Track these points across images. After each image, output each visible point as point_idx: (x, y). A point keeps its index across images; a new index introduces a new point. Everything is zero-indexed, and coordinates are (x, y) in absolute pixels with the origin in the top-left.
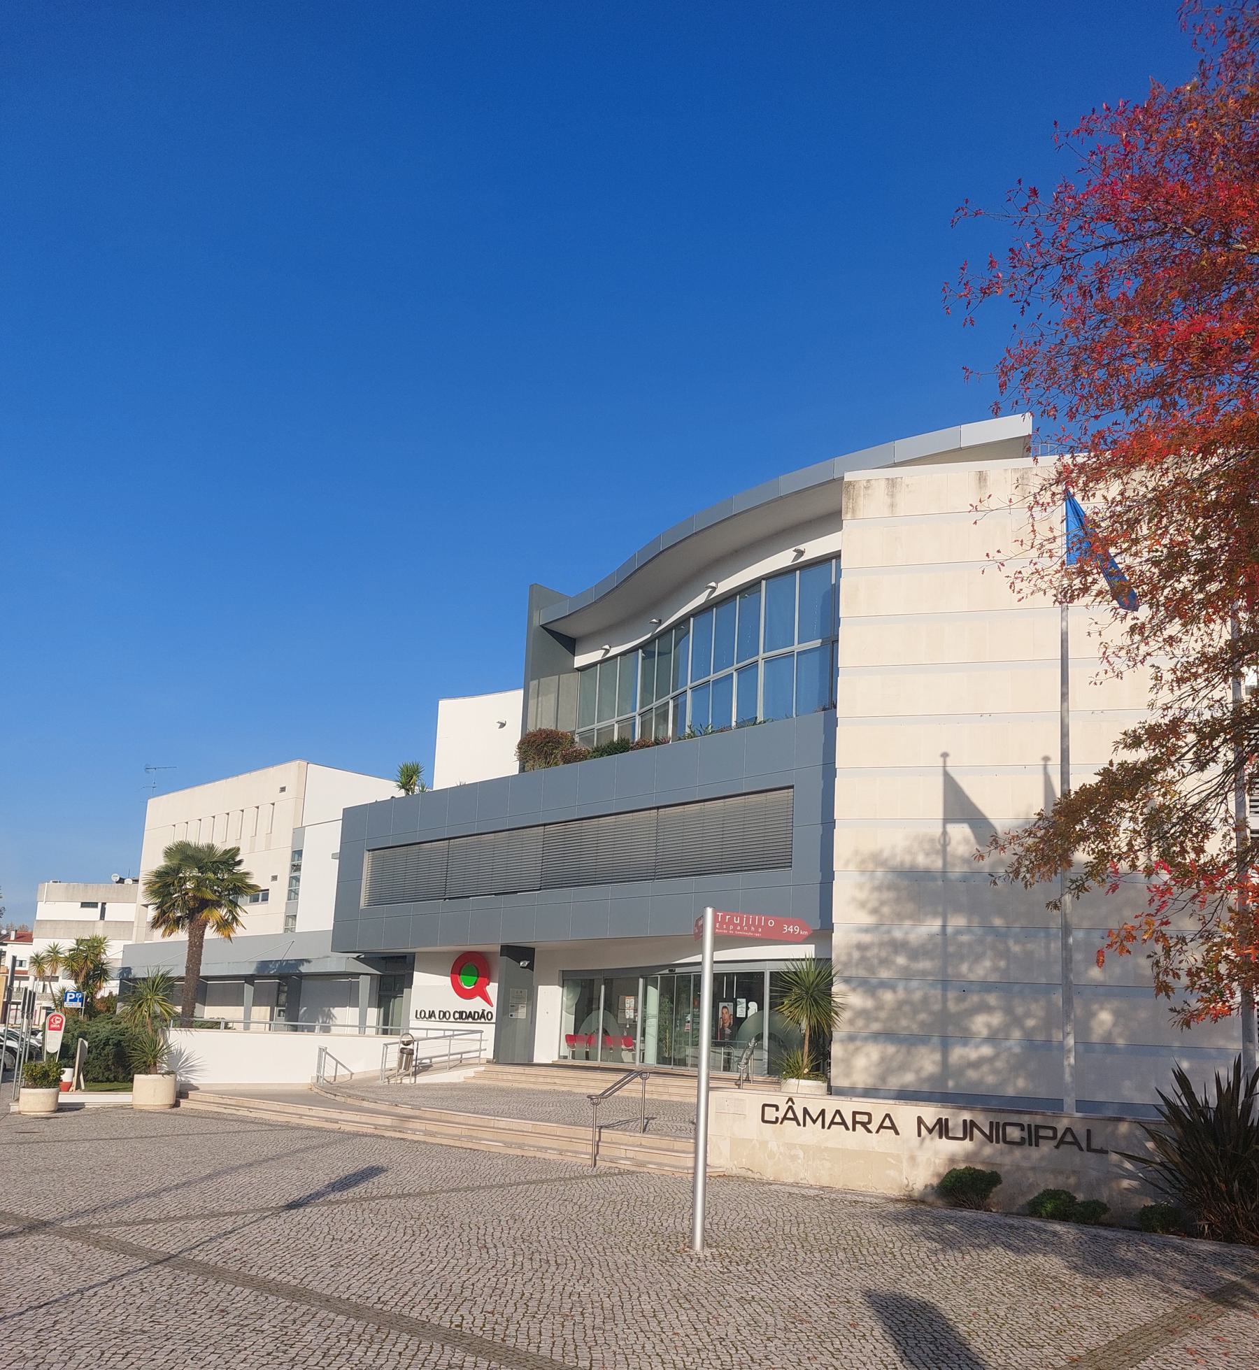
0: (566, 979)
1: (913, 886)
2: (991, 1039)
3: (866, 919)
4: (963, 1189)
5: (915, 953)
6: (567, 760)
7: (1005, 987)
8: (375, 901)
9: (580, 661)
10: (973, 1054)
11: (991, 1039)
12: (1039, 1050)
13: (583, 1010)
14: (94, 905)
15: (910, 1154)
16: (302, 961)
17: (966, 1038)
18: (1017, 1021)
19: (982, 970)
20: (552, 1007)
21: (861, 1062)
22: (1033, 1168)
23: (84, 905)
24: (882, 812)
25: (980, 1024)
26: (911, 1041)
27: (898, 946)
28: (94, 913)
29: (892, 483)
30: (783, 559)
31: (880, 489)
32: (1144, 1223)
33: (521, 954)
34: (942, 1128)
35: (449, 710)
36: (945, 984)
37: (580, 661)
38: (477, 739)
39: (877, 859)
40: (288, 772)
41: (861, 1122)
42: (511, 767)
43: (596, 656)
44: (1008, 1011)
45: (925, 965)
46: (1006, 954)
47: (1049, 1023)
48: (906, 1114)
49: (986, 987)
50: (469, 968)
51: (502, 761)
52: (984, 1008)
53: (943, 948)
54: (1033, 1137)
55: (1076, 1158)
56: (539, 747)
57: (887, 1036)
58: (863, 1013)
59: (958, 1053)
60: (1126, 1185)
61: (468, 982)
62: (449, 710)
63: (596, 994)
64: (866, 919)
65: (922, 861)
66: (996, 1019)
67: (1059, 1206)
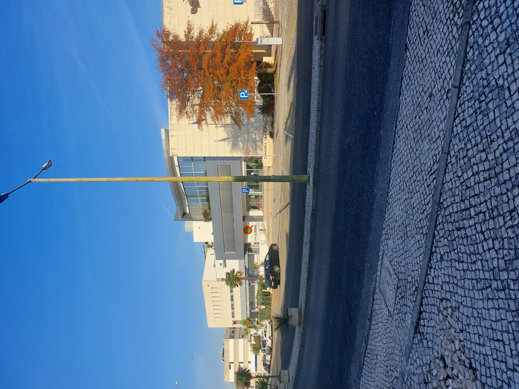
0: (248, 210)
1: (235, 146)
2: (255, 135)
3: (240, 152)
4: (272, 135)
5: (244, 145)
6: (210, 209)
7: (248, 133)
8: (234, 251)
9: (188, 212)
10: (258, 138)
11: (255, 135)
12: (256, 128)
13: (254, 208)
14: (230, 365)
15: (268, 141)
16: (245, 268)
17: (255, 138)
18: (253, 131)
19: (246, 136)
20: (253, 213)
21: (260, 153)
22: (269, 128)
23: (230, 369)
24: (224, 150)
25: (254, 137)
26: (256, 146)
27: (243, 148)
28: (232, 365)
29: (172, 149)
30: (177, 169)
31: (173, 151)
32: (273, 117)
33: (244, 218)
34: (266, 138)
35: (195, 240)
36: (248, 141)
37: (188, 212)
38: (202, 231)
39: (231, 151)
40: (204, 284)
41: (265, 147)
42: (211, 223)
43: (187, 207)
44: (252, 133)
45: (246, 144)
46: (244, 133)
47: (253, 127)
48: (264, 142)
49: (248, 136)
50: (247, 230)
51: (209, 226)
52: (251, 136)
53: (243, 141)
54: (266, 128)
55: (268, 124)
56: (207, 217)
57: (256, 149)
58: (253, 152)
59: (258, 139)
60: (270, 119)
61: (249, 230)
62: (195, 240)
63: (250, 207)
64: (240, 152)
65: (231, 145)
66: (253, 134)
67: (272, 125)
